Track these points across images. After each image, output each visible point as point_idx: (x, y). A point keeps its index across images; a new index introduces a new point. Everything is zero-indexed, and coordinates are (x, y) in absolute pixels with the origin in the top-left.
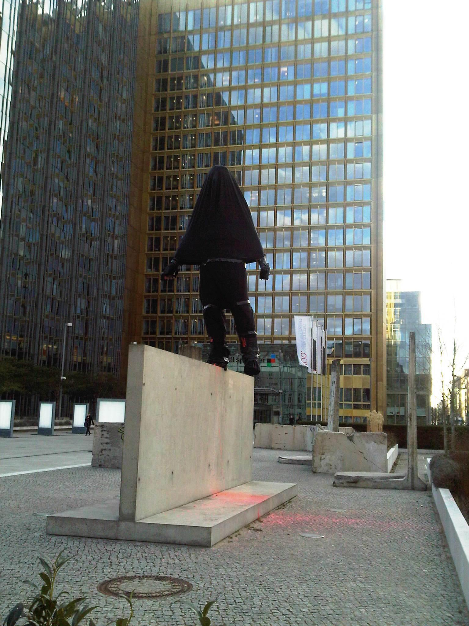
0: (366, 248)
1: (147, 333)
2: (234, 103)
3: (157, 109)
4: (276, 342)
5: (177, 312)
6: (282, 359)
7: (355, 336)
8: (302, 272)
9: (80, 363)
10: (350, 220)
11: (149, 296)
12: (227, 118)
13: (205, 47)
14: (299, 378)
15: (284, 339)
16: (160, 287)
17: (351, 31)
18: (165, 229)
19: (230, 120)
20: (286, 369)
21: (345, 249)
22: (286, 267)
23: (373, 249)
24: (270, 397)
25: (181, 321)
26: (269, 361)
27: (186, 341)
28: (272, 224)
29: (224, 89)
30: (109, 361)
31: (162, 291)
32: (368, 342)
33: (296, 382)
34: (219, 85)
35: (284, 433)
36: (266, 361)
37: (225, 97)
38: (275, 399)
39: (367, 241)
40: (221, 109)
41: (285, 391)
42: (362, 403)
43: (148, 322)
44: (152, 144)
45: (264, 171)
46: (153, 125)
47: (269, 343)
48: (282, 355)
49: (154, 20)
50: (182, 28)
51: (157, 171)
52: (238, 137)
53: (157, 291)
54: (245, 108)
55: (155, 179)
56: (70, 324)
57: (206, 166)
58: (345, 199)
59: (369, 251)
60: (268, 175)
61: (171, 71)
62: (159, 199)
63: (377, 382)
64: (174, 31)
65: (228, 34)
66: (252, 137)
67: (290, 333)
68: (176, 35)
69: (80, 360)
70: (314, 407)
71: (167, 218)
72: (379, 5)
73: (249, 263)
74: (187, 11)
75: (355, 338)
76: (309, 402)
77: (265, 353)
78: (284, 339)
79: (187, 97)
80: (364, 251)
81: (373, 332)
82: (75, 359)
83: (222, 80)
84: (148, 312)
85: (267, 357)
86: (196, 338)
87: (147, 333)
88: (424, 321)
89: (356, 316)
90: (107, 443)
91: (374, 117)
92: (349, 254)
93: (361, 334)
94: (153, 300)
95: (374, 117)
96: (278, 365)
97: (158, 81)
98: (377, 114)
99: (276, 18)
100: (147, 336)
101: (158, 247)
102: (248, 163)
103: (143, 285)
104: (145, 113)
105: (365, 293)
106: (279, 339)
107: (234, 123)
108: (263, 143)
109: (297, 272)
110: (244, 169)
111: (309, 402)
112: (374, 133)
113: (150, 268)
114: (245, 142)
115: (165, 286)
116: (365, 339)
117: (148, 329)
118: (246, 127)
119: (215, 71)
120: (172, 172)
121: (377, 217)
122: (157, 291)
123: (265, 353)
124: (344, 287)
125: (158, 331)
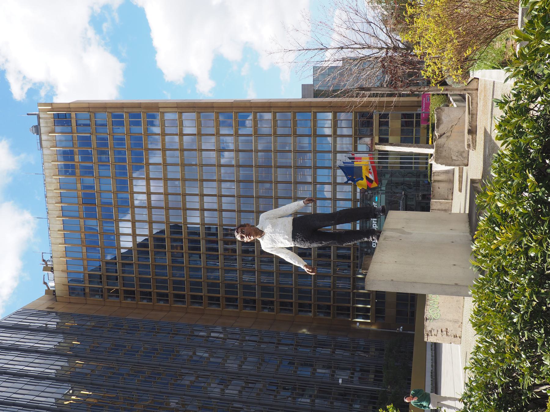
0: (274, 117)
2: (147, 232)
4: (358, 196)
5: (330, 287)
9: (375, 376)
14: (391, 176)
18: (255, 295)
19: (161, 236)
21: (335, 135)
24: (409, 203)
27: (356, 279)
28: (162, 197)
29: (134, 240)
30: (374, 350)
31: (311, 300)
33: (394, 179)
34: (130, 245)
37: (140, 240)
38: (411, 198)
41: (404, 190)
42: (415, 119)
43: (300, 311)
45: (224, 208)
49: (74, 299)
51: (294, 308)
52: (176, 229)
53: (310, 305)
54: (151, 222)
57: (200, 258)
59: (277, 114)
60: (210, 202)
61: (273, 298)
69: (373, 376)
70: (418, 163)
75: (355, 126)
76: (413, 168)
80: (277, 118)
82: (372, 380)
89: (295, 124)
91: (161, 110)
93: (352, 120)
94: (337, 310)
95: (161, 110)
97: (126, 298)
100: (351, 314)
102: (216, 221)
107: (162, 232)
108: (147, 205)
110: (222, 225)
111: (413, 168)
112: (175, 110)
114: (181, 223)
116: (355, 117)
118: (168, 222)
120: (222, 290)
121: (247, 107)
124: (309, 136)
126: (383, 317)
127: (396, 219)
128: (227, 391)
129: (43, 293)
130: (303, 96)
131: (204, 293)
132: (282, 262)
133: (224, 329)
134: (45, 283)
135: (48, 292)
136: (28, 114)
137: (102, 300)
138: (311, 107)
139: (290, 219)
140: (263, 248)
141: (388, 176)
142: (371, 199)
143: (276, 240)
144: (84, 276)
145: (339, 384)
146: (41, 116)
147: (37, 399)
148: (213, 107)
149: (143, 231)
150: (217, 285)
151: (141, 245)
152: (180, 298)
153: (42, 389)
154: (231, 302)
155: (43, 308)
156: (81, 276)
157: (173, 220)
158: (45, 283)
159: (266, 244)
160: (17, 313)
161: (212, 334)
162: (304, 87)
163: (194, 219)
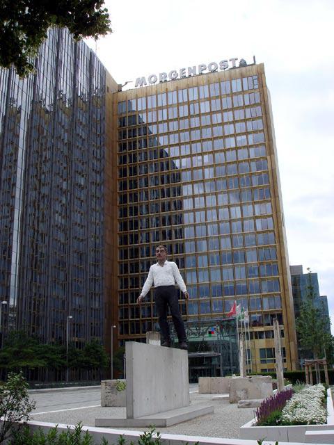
1: (122, 318)
6: (219, 331)
9: (77, 342)
10: (248, 116)
11: (122, 262)
12: (169, 164)
13: (150, 121)
16: (130, 284)
17: (246, 88)
23: (272, 202)
25: (144, 235)
26: (210, 333)
31: (131, 287)
39: (260, 114)
40: (164, 160)
44: (118, 186)
46: (118, 173)
48: (218, 328)
50: (134, 109)
52: (177, 177)
55: (122, 280)
56: (71, 317)
58: (254, 214)
64: (129, 112)
65: (165, 111)
66: (186, 176)
68: (130, 114)
71: (131, 236)
74: (137, 99)
79: (142, 263)
83: (162, 141)
84: (121, 288)
87: (122, 318)
88: (322, 294)
92: (258, 222)
95: (268, 157)
99: (196, 98)
101: (125, 148)
103: (118, 285)
104: (113, 166)
115: (133, 283)
119: (158, 135)
125: (129, 302)
127: (181, 357)
128: (56, 215)
129: (118, 84)
130: (291, 267)
132: (144, 281)
133: (103, 223)
134: (126, 83)
135: (120, 86)
139: (173, 283)
140: (152, 266)
141: (233, 340)
142: (176, 343)
143: (163, 274)
144: (134, 111)
145: (68, 315)
147: (42, 75)
148: (275, 197)
149: (174, 152)
150: (136, 213)
151: (162, 152)
152: (124, 186)
153: (50, 62)
154: (124, 226)
155: (108, 84)
156: (134, 109)
157: (183, 174)
158: (126, 83)
159: (155, 268)
160: (102, 67)
161: (98, 214)
162: (300, 267)
163: (187, 190)
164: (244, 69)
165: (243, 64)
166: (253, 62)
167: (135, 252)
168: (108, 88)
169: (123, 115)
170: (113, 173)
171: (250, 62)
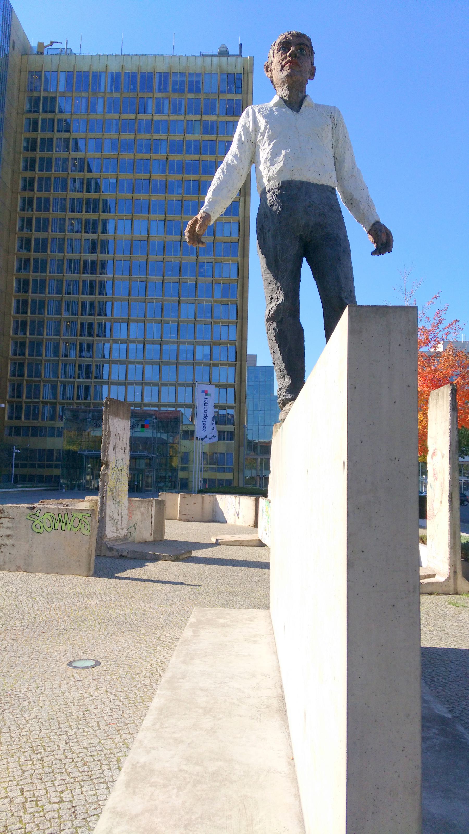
3: (25, 169)
7: (221, 404)
8: (138, 342)
15: (170, 406)
20: (159, 435)
22: (124, 336)
32: (231, 412)
35: (193, 503)
36: (140, 426)
47: (139, 409)
62: (27, 261)
63: (239, 447)
67: (193, 401)
68: (46, 94)
72: (250, 91)
73: (417, 317)
77: (138, 419)
78: (170, 406)
81: (237, 401)
85: (140, 423)
86: (82, 403)
90: (8, 536)
93: (226, 403)
96: (151, 431)
98: (245, 197)
100: (13, 400)
104: (13, 172)
105: (231, 365)
106: (165, 406)
109: (133, 342)
113: (100, 325)
117: (12, 413)
122: (24, 355)
123: (138, 419)
126: (10, 435)
131: (31, 296)
136: (241, 44)
137: (25, 110)
138: (241, 361)
146: (239, 60)
155: (14, 36)
164: (224, 59)
165: (224, 53)
166: (238, 54)
167: (40, 306)
168: (14, 43)
169: (35, 94)
170: (13, 182)
171: (233, 51)
